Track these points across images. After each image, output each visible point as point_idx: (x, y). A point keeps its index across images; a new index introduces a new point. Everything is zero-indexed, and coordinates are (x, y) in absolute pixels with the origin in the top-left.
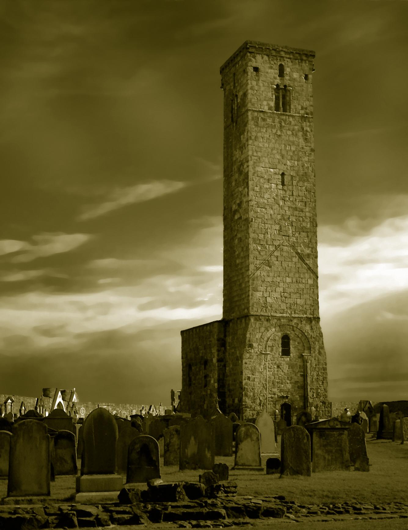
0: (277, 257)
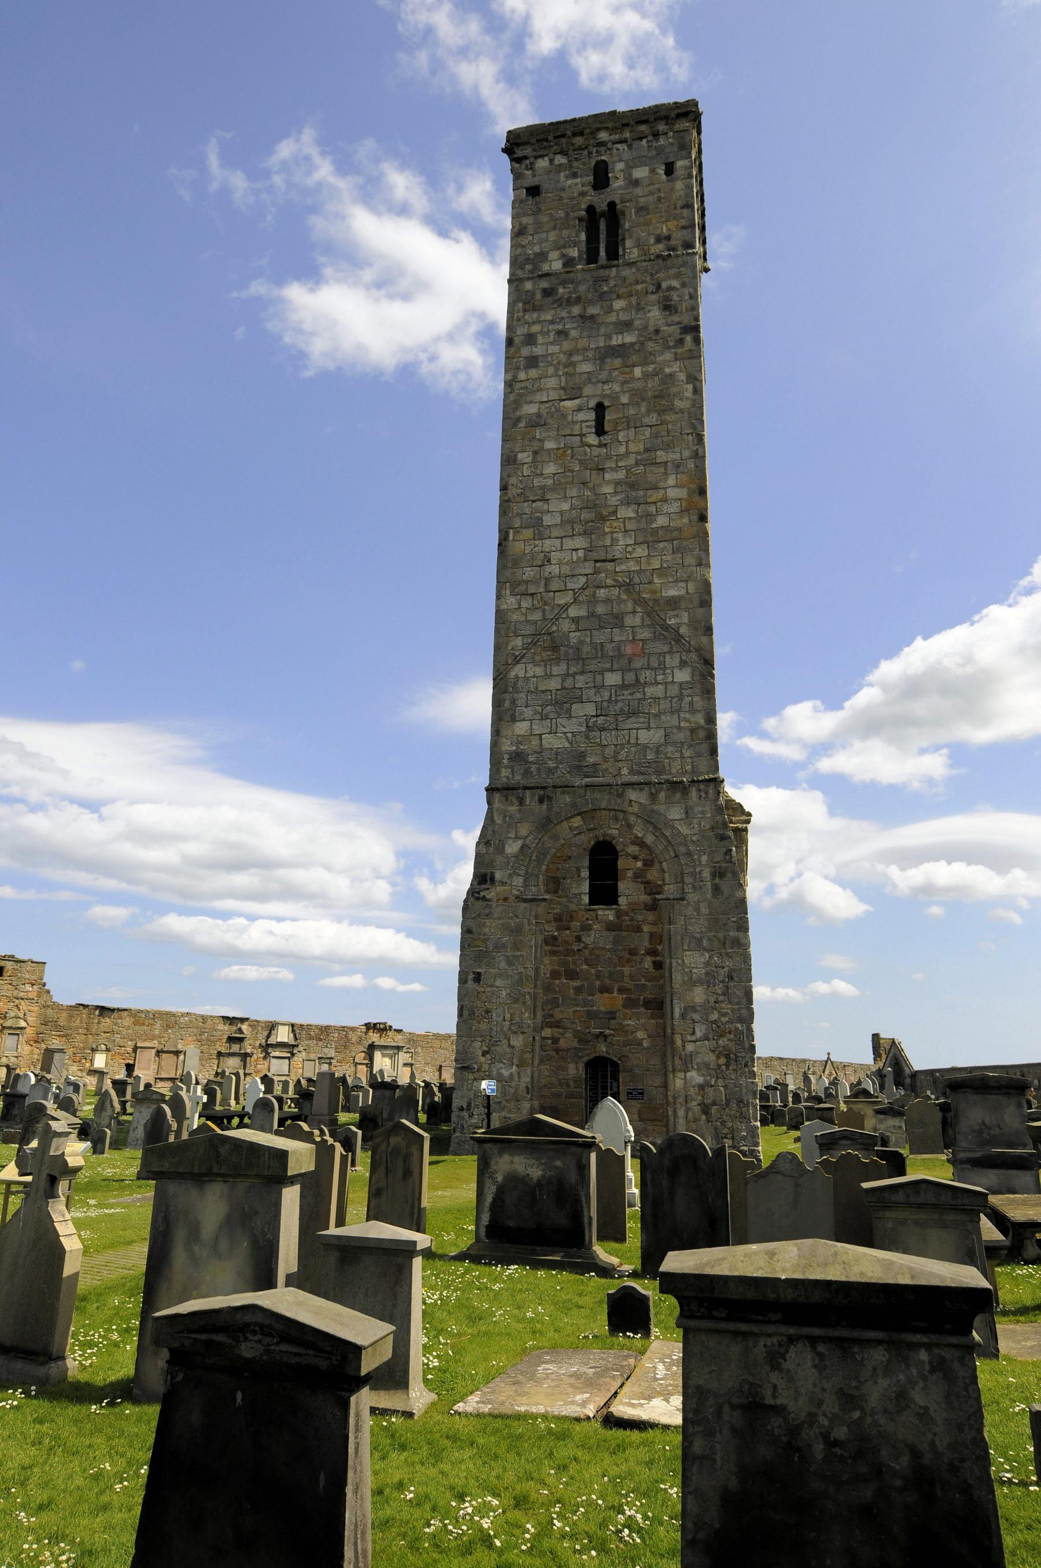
0: (576, 620)
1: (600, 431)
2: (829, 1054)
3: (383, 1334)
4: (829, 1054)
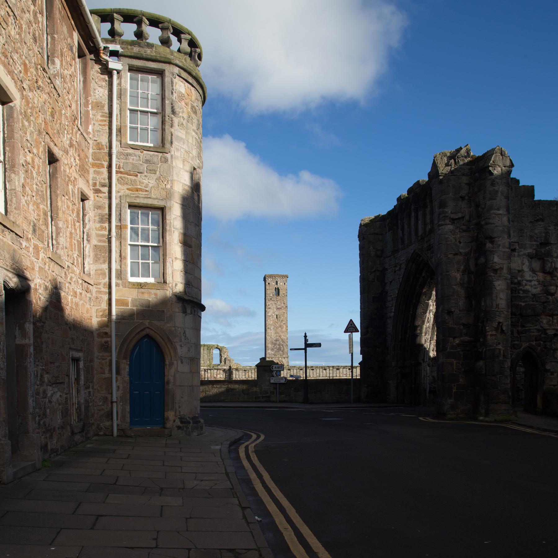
1: (277, 318)
2: (319, 345)
3: (8, 226)
4: (319, 345)
